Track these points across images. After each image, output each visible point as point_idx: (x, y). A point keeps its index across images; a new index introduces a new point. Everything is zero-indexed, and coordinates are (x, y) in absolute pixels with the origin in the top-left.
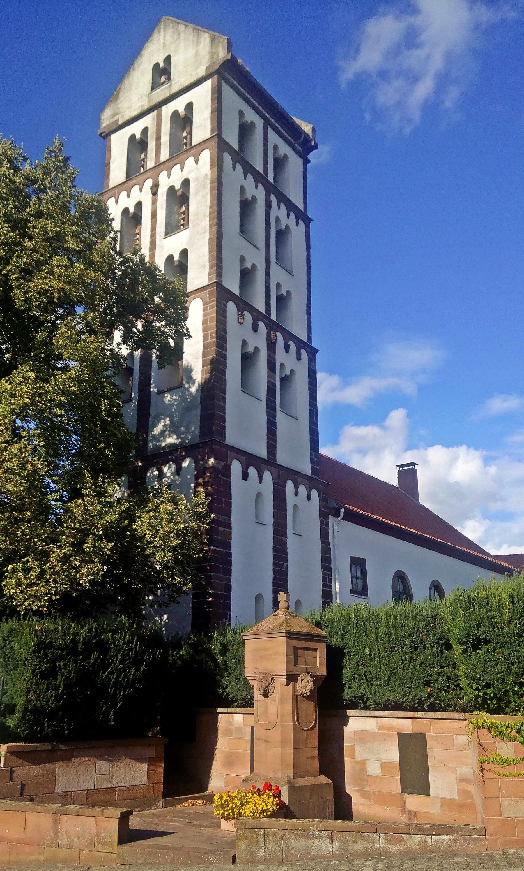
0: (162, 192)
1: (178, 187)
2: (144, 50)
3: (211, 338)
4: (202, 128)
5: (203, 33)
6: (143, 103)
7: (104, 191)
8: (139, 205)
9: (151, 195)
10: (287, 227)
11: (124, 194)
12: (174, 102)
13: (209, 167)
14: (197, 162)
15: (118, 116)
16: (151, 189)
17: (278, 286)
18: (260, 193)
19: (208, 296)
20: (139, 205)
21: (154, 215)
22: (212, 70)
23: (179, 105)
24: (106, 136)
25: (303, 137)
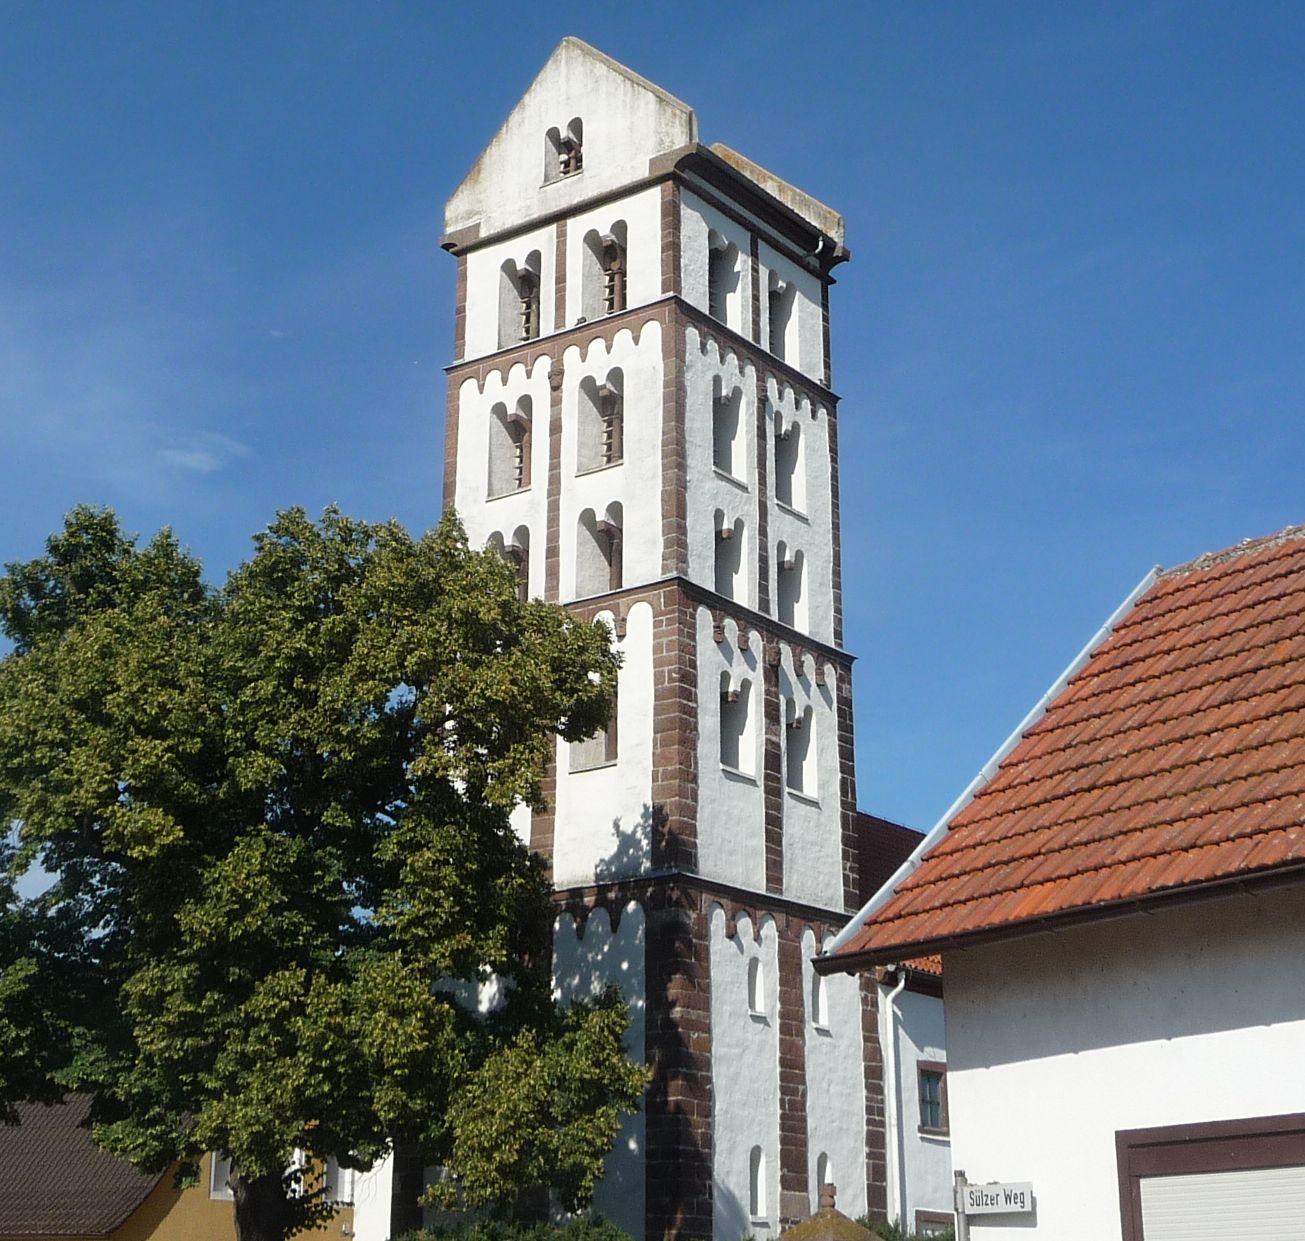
3: (671, 680)
4: (644, 283)
7: (457, 363)
8: (526, 402)
10: (796, 426)
12: (656, 460)
14: (636, 340)
15: (477, 217)
17: (781, 547)
20: (526, 402)
21: (556, 428)
23: (601, 221)
24: (459, 250)
25: (821, 244)
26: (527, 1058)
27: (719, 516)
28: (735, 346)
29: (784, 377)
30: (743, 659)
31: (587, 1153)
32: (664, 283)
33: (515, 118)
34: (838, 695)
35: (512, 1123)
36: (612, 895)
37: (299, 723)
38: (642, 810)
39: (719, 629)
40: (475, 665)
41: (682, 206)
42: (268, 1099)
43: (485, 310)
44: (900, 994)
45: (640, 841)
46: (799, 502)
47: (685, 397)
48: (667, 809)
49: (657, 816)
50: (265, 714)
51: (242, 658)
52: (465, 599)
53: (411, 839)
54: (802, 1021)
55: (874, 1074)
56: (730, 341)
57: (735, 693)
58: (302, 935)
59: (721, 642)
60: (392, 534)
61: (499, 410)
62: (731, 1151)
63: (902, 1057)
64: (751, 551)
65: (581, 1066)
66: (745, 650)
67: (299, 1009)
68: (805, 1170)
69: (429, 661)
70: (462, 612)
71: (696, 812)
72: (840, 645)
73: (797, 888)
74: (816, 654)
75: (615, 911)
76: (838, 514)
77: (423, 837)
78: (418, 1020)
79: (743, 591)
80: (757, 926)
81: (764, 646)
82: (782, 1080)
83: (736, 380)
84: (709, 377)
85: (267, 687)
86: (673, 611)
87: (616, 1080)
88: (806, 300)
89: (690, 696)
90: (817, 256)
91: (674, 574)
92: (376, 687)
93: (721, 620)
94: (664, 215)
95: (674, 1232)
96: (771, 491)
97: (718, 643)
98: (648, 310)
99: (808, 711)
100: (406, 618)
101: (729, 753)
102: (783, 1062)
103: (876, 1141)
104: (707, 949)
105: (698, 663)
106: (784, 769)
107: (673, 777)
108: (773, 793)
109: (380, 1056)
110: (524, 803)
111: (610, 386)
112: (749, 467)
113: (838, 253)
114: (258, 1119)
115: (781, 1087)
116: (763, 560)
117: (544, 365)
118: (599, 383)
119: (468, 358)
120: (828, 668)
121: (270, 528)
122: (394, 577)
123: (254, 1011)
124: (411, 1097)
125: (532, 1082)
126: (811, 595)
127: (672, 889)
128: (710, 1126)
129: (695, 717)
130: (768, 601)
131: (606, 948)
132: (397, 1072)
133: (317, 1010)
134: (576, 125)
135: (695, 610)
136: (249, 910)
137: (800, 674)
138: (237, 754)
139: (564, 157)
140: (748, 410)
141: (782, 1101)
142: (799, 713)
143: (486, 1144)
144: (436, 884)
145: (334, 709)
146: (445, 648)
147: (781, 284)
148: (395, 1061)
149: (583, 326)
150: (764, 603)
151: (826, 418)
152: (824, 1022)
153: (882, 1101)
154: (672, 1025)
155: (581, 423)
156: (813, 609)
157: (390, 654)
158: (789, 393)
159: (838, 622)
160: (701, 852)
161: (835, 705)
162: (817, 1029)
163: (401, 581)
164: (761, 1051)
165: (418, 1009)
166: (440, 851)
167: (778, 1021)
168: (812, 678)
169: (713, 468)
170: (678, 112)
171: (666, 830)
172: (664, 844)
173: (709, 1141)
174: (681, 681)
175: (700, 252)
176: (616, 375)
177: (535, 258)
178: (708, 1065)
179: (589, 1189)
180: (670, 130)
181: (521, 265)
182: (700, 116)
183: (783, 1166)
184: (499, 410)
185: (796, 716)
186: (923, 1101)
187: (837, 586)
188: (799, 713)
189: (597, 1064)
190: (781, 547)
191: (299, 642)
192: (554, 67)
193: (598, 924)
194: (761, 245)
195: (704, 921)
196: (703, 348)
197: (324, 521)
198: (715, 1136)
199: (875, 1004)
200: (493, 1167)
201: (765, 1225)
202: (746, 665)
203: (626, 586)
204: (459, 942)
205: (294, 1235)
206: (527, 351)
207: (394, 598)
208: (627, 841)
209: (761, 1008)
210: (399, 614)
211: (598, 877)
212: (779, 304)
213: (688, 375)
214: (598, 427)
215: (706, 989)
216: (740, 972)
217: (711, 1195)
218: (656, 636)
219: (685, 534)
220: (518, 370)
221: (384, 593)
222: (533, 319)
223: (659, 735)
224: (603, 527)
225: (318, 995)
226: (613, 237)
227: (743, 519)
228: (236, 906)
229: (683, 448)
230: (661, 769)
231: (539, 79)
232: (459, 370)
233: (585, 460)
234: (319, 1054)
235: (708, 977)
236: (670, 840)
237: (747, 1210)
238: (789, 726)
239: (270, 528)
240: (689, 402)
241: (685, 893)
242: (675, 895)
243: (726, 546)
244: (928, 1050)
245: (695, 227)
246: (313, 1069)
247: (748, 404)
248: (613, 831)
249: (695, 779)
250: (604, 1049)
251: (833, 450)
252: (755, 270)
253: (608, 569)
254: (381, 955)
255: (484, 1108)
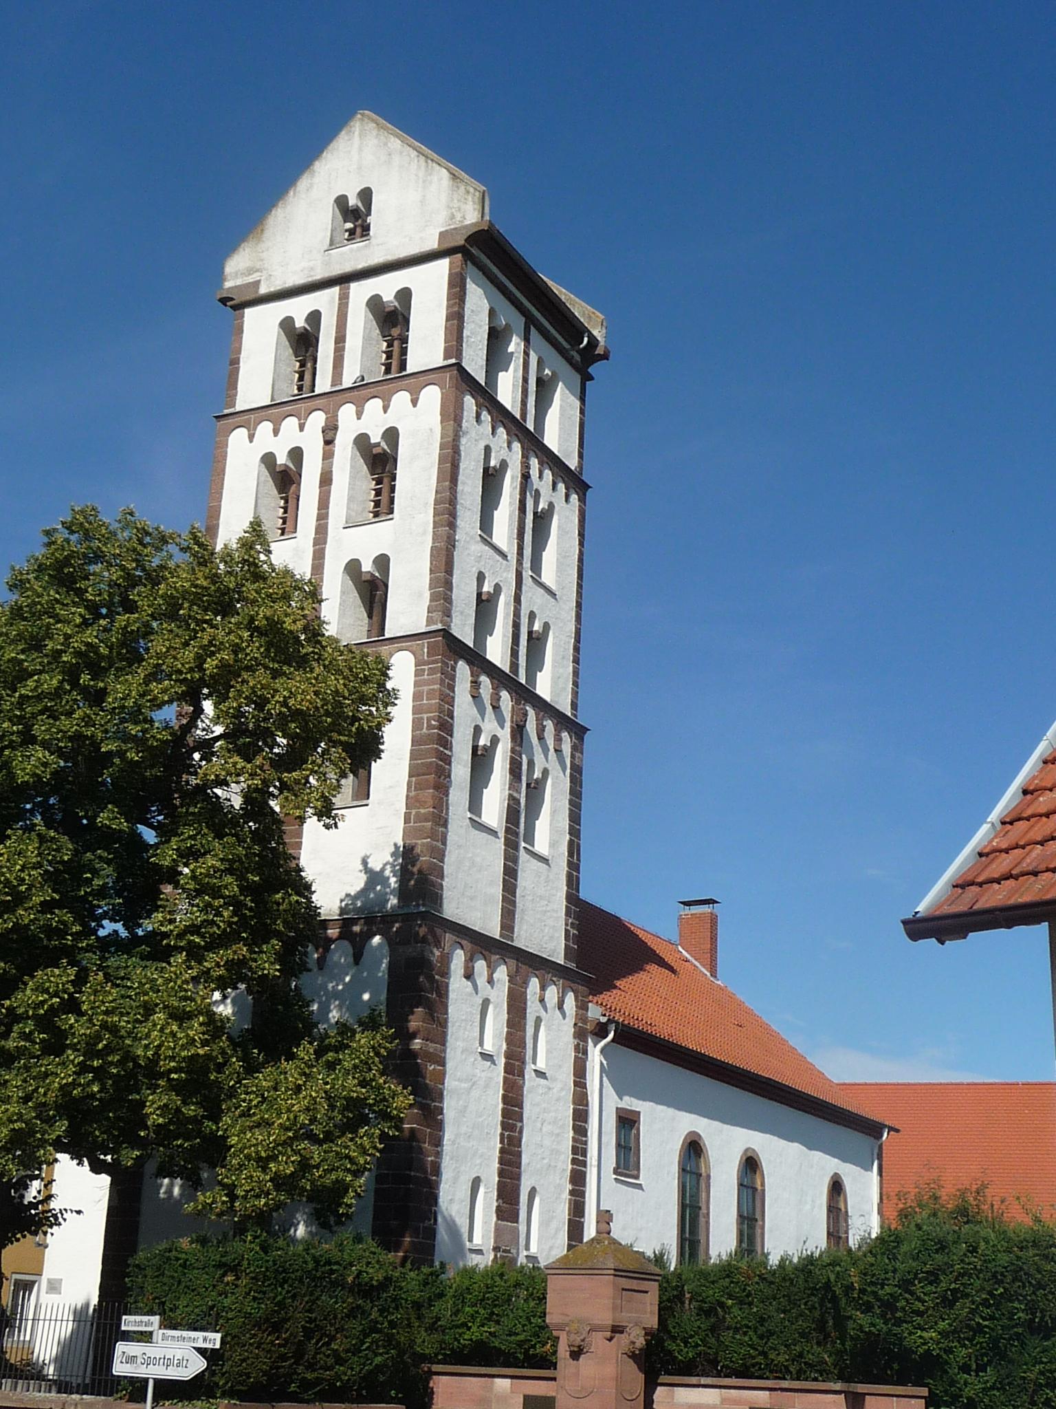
2: (317, 163)
3: (430, 727)
4: (426, 348)
6: (311, 264)
7: (226, 411)
8: (296, 454)
11: (266, 427)
12: (426, 518)
13: (439, 418)
14: (414, 402)
17: (532, 616)
20: (296, 454)
21: (326, 480)
23: (387, 287)
24: (237, 304)
25: (586, 340)
26: (307, 1071)
27: (481, 578)
31: (349, 1170)
32: (446, 350)
33: (303, 183)
35: (290, 1134)
36: (357, 929)
37: (83, 720)
38: (393, 849)
39: (476, 684)
40: (276, 674)
42: (26, 1099)
43: (260, 364)
44: (608, 1043)
45: (388, 878)
47: (459, 460)
48: (418, 850)
49: (407, 855)
50: (46, 709)
51: (23, 652)
53: (192, 846)
54: (524, 1062)
55: (581, 1116)
56: (501, 415)
58: (71, 935)
59: (476, 697)
60: (195, 538)
61: (268, 460)
62: (456, 1179)
63: (605, 1103)
64: (507, 615)
65: (350, 1086)
66: (496, 708)
67: (72, 1006)
68: (518, 1203)
69: (230, 666)
70: (267, 619)
71: (444, 855)
72: (575, 716)
73: (524, 939)
75: (359, 946)
77: (203, 846)
78: (201, 1024)
79: (497, 650)
80: (491, 969)
82: (503, 1116)
83: (504, 453)
84: (482, 445)
85: (52, 681)
87: (381, 1101)
89: (447, 744)
90: (580, 352)
91: (440, 626)
92: (172, 687)
93: (478, 676)
94: (451, 285)
95: (401, 1254)
96: (527, 563)
99: (545, 772)
101: (475, 804)
102: (505, 1099)
103: (578, 1179)
104: (447, 985)
105: (455, 714)
106: (522, 820)
107: (427, 820)
108: (511, 845)
109: (154, 1061)
110: (315, 818)
111: (383, 444)
112: (510, 537)
113: (600, 351)
114: (20, 1117)
115: (502, 1123)
116: (516, 626)
117: (317, 420)
119: (238, 408)
121: (63, 523)
123: (19, 1007)
124: (185, 1103)
125: (314, 1094)
126: (554, 667)
127: (420, 926)
128: (439, 1154)
129: (450, 764)
130: (517, 665)
131: (347, 979)
132: (174, 1076)
133: (92, 1008)
134: (366, 195)
135: (456, 663)
136: (22, 903)
137: (541, 738)
138: (12, 746)
139: (349, 225)
141: (502, 1135)
143: (263, 1154)
144: (216, 892)
145: (123, 707)
146: (247, 655)
147: (547, 371)
148: (172, 1064)
150: (514, 666)
151: (577, 503)
152: (541, 1064)
153: (586, 1143)
154: (413, 1055)
155: (353, 477)
156: (555, 679)
157: (189, 654)
158: (548, 474)
159: (575, 694)
160: (446, 894)
161: (568, 771)
162: (535, 1071)
163: (205, 584)
164: (487, 1086)
165: (201, 1013)
166: (222, 860)
167: (503, 1060)
168: (551, 743)
170: (472, 190)
171: (415, 870)
172: (412, 882)
173: (437, 1170)
175: (481, 327)
176: (392, 435)
177: (314, 318)
178: (440, 1097)
179: (350, 1206)
180: (463, 207)
182: (494, 195)
183: (499, 1196)
184: (268, 460)
186: (618, 1145)
187: (576, 661)
189: (363, 1083)
190: (532, 616)
191: (90, 636)
193: (340, 955)
194: (533, 330)
195: (446, 960)
197: (120, 522)
198: (443, 1165)
199: (585, 1052)
200: (268, 1178)
201: (479, 1252)
204: (235, 952)
205: (18, 1240)
206: (302, 406)
207: (196, 599)
208: (374, 878)
209: (489, 1047)
210: (199, 617)
211: (343, 911)
212: (545, 389)
213: (463, 441)
215: (443, 1024)
216: (474, 1009)
217: (436, 1220)
218: (416, 684)
219: (451, 589)
221: (185, 594)
222: (307, 377)
224: (368, 577)
225: (95, 992)
228: (9, 898)
230: (414, 812)
231: (330, 148)
232: (229, 419)
233: (353, 514)
234: (91, 1052)
235: (446, 1013)
236: (418, 876)
237: (466, 1236)
238: (528, 785)
239: (63, 523)
240: (462, 466)
241: (431, 931)
242: (423, 931)
243: (485, 606)
244: (626, 1098)
245: (478, 300)
246: (83, 1069)
247: (513, 478)
248: (361, 867)
249: (445, 825)
250: (370, 1070)
252: (526, 354)
253: (366, 620)
254: (144, 963)
255: (262, 1118)
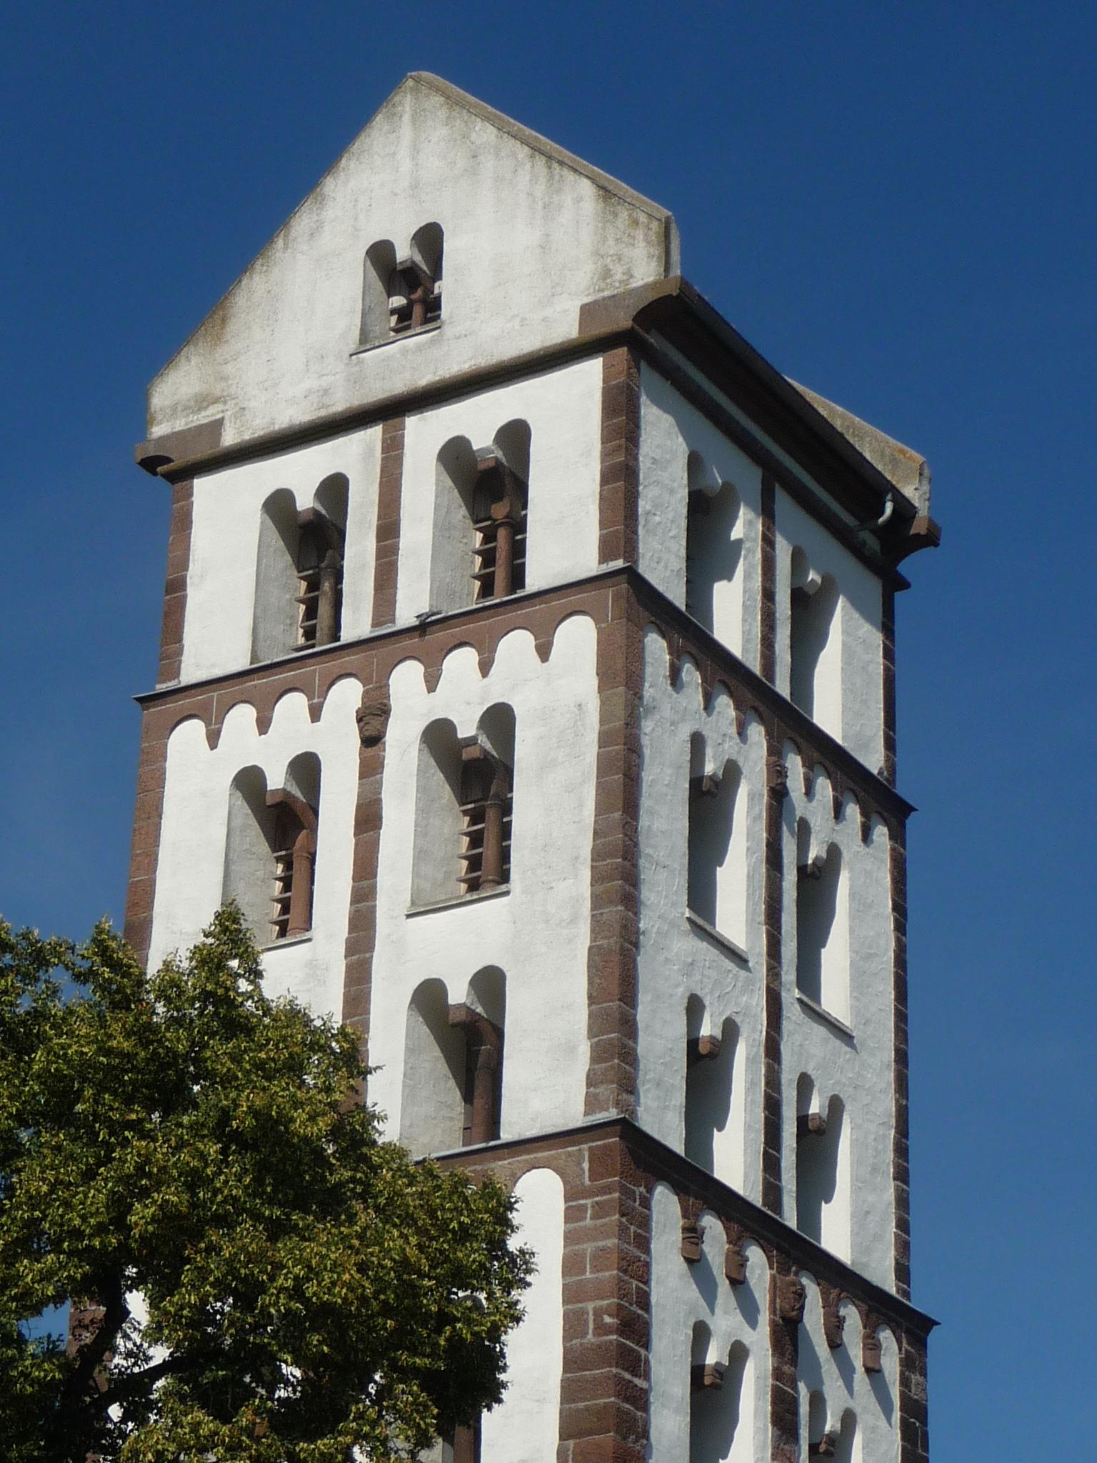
0: (403, 738)
1: (467, 728)
3: (601, 1329)
4: (563, 541)
5: (570, 176)
6: (325, 382)
7: (161, 687)
8: (306, 768)
9: (357, 742)
10: (834, 852)
12: (579, 885)
13: (594, 682)
14: (544, 651)
15: (219, 407)
16: (359, 720)
18: (754, 750)
19: (586, 1165)
20: (306, 768)
21: (368, 819)
22: (601, 328)
23: (477, 422)
24: (178, 469)
27: (694, 1008)
28: (733, 683)
29: (816, 755)
30: (733, 1303)
33: (302, 222)
34: (902, 1395)
39: (693, 1234)
40: (277, 1230)
41: (644, 399)
43: (226, 591)
46: (835, 996)
52: (264, 1089)
56: (722, 670)
57: (718, 1368)
59: (695, 1261)
66: (738, 1283)
74: (865, 1307)
76: (905, 1033)
79: (734, 1160)
81: (773, 1278)
83: (731, 748)
86: (607, 1190)
88: (856, 615)
91: (612, 1114)
92: (63, 1267)
93: (698, 1217)
96: (789, 974)
97: (689, 1261)
98: (570, 597)
99: (849, 1419)
100: (130, 1125)
105: (653, 1299)
111: (484, 741)
112: (750, 922)
113: (919, 527)
116: (773, 1107)
118: (463, 733)
120: (886, 1337)
122: (110, 1037)
126: (856, 1190)
134: (430, 238)
135: (650, 1190)
137: (835, 1344)
139: (398, 301)
140: (750, 808)
142: (831, 1424)
146: (216, 1192)
147: (812, 575)
149: (424, 627)
150: (772, 1191)
156: (860, 1217)
157: (97, 1196)
158: (824, 788)
159: (903, 1247)
161: (897, 1415)
168: (856, 1354)
169: (687, 913)
170: (643, 218)
174: (621, 1333)
175: (672, 492)
176: (500, 720)
177: (335, 489)
180: (627, 252)
181: (305, 501)
182: (688, 224)
185: (827, 1428)
187: (902, 1175)
188: (831, 1424)
190: (805, 1085)
192: (386, 127)
196: (675, 677)
202: (740, 1317)
203: (506, 1135)
206: (315, 669)
207: (108, 1079)
210: (115, 1116)
212: (809, 615)
213: (647, 726)
214: (453, 825)
218: (569, 1238)
220: (293, 706)
221: (85, 1068)
222: (324, 609)
223: (571, 1443)
224: (459, 1017)
226: (499, 454)
227: (738, 1020)
229: (635, 866)
240: (647, 776)
243: (706, 1068)
245: (664, 440)
247: (752, 797)
251: (900, 909)
252: (768, 542)
